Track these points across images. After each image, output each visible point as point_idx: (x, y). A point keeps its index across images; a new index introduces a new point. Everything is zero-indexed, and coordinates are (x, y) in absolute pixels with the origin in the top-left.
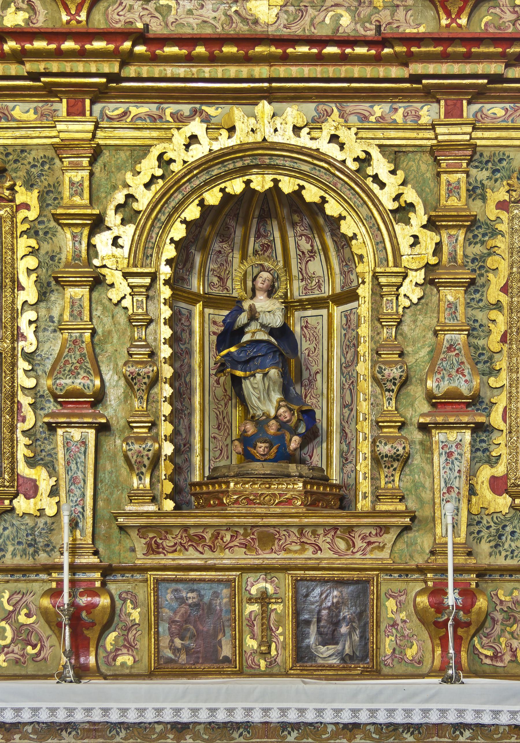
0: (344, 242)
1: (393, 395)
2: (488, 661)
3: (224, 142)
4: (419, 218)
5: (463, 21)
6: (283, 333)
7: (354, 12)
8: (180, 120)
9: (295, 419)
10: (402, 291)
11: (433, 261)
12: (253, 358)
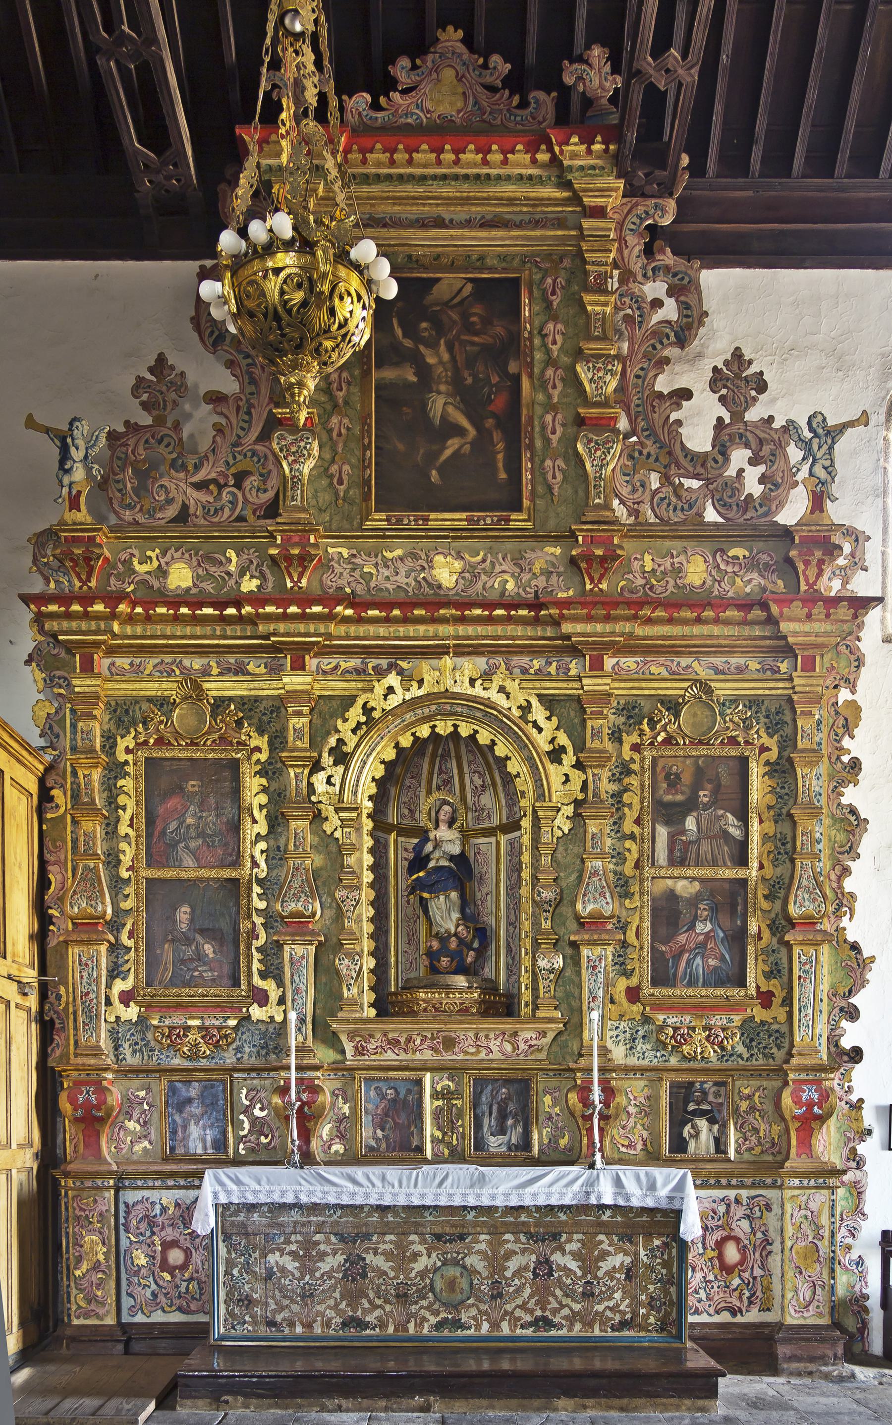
0: (509, 779)
1: (549, 915)
2: (623, 1150)
3: (416, 692)
4: (569, 759)
5: (604, 586)
6: (461, 860)
7: (517, 578)
8: (381, 673)
9: (470, 937)
10: (557, 822)
11: (581, 796)
12: (437, 882)
